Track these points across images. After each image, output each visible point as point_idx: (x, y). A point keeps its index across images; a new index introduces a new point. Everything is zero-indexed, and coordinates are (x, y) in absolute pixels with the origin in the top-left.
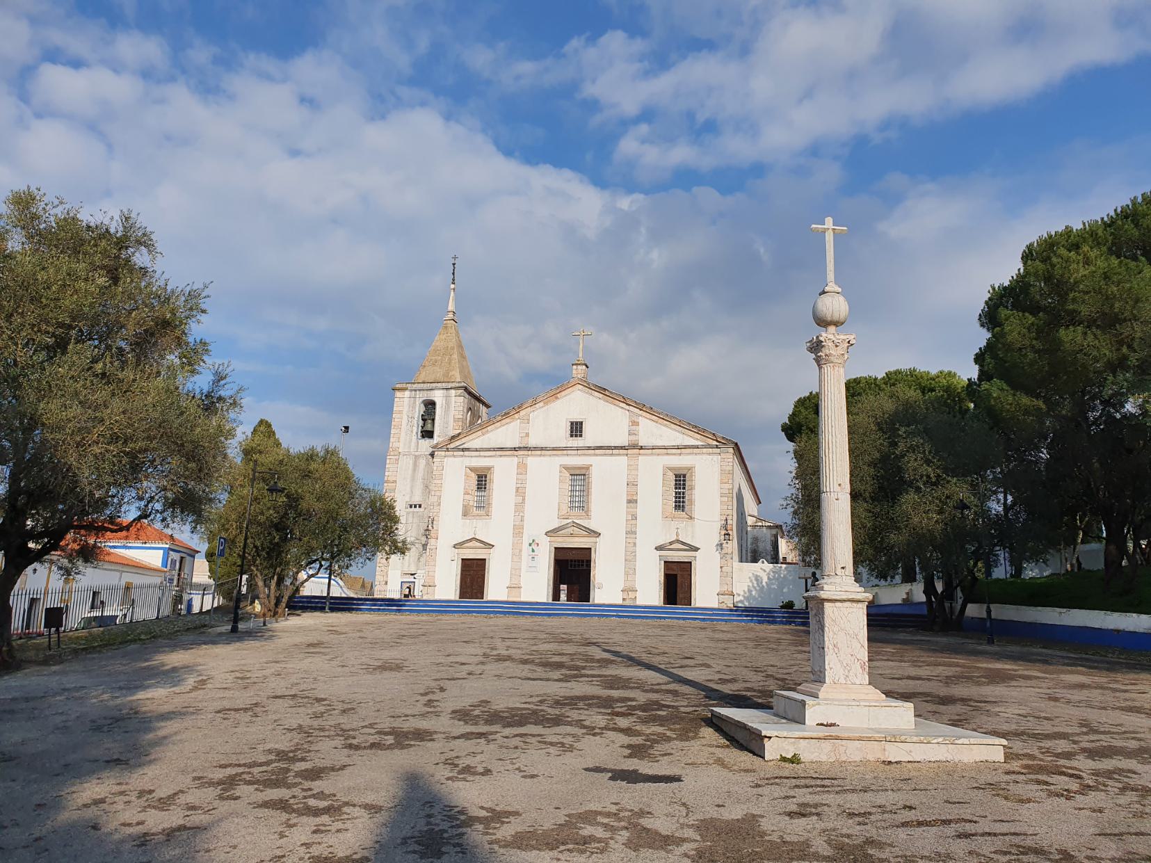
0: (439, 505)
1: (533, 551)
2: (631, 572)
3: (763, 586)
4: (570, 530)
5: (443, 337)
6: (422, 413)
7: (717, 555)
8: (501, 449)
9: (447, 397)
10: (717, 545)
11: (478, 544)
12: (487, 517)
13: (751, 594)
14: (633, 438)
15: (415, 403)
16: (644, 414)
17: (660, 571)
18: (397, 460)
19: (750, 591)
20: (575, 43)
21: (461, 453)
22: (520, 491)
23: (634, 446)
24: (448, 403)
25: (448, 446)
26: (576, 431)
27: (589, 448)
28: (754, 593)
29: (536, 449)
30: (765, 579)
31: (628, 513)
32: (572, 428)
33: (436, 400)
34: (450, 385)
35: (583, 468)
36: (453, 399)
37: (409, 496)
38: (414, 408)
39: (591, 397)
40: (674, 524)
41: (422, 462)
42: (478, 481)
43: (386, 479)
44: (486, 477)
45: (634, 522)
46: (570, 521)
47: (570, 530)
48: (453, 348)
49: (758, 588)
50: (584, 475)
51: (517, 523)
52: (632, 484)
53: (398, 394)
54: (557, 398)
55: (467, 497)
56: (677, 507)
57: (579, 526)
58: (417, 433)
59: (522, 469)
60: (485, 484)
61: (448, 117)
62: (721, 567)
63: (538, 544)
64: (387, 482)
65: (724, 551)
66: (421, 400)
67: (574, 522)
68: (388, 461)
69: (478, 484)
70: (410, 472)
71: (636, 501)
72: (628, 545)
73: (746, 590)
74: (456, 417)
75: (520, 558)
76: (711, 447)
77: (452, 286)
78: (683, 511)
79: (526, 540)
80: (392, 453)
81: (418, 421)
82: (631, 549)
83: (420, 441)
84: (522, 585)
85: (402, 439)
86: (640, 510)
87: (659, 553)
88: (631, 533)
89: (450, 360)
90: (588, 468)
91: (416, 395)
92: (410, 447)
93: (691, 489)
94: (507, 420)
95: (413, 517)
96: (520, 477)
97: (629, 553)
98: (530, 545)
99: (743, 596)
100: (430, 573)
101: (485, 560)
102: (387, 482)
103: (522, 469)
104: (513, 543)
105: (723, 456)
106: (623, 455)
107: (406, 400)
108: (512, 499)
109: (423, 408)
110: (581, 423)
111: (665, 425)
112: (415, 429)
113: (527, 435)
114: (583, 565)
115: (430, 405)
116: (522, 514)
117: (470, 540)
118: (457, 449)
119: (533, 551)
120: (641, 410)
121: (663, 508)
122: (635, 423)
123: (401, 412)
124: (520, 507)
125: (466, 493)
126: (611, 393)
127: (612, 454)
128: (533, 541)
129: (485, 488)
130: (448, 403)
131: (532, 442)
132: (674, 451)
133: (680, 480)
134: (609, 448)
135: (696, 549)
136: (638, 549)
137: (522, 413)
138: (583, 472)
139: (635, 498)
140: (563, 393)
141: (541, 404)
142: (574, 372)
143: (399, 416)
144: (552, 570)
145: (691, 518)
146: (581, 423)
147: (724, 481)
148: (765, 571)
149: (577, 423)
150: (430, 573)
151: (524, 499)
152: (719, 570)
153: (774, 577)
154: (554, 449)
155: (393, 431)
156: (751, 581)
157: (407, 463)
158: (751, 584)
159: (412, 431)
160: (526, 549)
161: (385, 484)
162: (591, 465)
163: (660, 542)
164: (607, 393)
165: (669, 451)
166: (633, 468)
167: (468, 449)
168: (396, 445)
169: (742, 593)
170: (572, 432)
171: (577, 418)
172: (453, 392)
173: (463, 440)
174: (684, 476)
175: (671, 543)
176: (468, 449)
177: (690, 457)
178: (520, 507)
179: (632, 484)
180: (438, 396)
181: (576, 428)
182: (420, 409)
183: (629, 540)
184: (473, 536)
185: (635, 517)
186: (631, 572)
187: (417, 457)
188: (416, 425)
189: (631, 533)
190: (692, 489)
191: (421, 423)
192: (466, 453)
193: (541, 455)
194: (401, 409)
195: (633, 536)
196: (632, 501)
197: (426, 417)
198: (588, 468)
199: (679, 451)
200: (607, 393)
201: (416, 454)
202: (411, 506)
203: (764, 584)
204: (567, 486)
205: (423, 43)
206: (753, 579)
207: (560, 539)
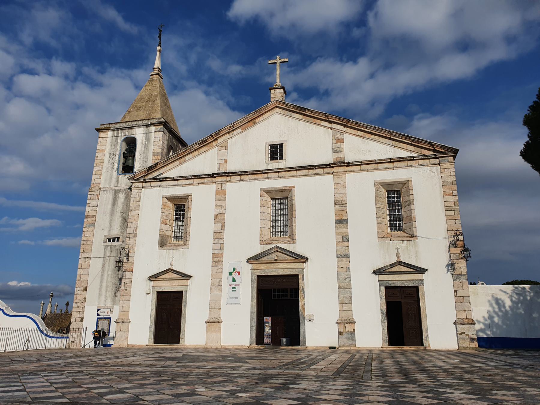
0: (135, 236)
1: (234, 280)
2: (346, 300)
3: (506, 311)
4: (274, 256)
5: (148, 88)
6: (124, 150)
7: (449, 277)
8: (199, 177)
9: (148, 133)
10: (448, 265)
11: (175, 276)
12: (184, 247)
13: (493, 322)
14: (338, 155)
15: (116, 141)
16: (349, 130)
17: (381, 298)
18: (98, 195)
19: (491, 317)
20: (260, 59)
21: (159, 183)
22: (219, 218)
23: (340, 163)
24: (148, 139)
25: (146, 178)
26: (276, 155)
27: (291, 169)
28: (496, 319)
29: (235, 174)
30: (508, 303)
31: (337, 235)
32: (271, 151)
33: (137, 136)
34: (149, 122)
35: (285, 190)
36: (153, 135)
37: (108, 229)
38: (116, 145)
39: (290, 119)
40: (394, 244)
41: (122, 197)
42: (176, 211)
43: (86, 214)
44: (184, 207)
45: (345, 244)
46: (274, 245)
47: (274, 256)
48: (156, 96)
49: (500, 314)
50: (286, 198)
51: (216, 252)
52: (340, 203)
53: (102, 134)
54: (255, 123)
55: (165, 227)
56: (393, 227)
57: (284, 251)
58: (118, 169)
59: (221, 194)
60: (184, 214)
61: (207, 93)
62: (455, 291)
63: (239, 273)
64: (88, 217)
65: (456, 272)
66: (123, 138)
67: (278, 247)
68: (89, 197)
69: (176, 215)
70: (110, 206)
71: (346, 221)
72: (341, 270)
73: (486, 315)
74: (156, 151)
75: (220, 290)
76: (428, 158)
77: (158, 48)
78: (400, 230)
79: (226, 269)
80: (93, 189)
81: (119, 157)
82: (344, 274)
83: (120, 177)
84: (222, 319)
85: (103, 176)
86: (352, 231)
87: (377, 278)
88: (343, 256)
89: (153, 106)
90: (289, 190)
91: (118, 134)
92: (110, 182)
93: (410, 204)
94: (205, 148)
95: (111, 251)
96: (219, 203)
97: (343, 279)
98: (231, 274)
99: (484, 324)
100: (125, 309)
101: (182, 292)
102: (88, 217)
103: (221, 194)
104: (212, 272)
105: (443, 166)
106: (328, 173)
107: (109, 140)
108: (211, 226)
109: (125, 147)
110: (281, 145)
111: (374, 140)
112: (116, 166)
113: (226, 161)
114: (286, 295)
115: (131, 143)
116: (221, 241)
117: (166, 272)
118: (155, 179)
119: (234, 280)
120: (345, 126)
121: (378, 227)
122: (339, 141)
123: (103, 151)
124: (219, 235)
125: (163, 223)
126: (311, 111)
127: (315, 175)
128: (234, 269)
129: (183, 218)
130: (148, 139)
131: (231, 168)
132: (386, 165)
133: (394, 197)
134: (312, 167)
135: (423, 271)
136: (352, 274)
137: (220, 140)
138: (284, 195)
139: (344, 218)
140: (261, 118)
141: (239, 130)
142: (272, 96)
143: (101, 154)
144: (255, 301)
145: (412, 236)
146: (281, 145)
147: (447, 193)
148: (505, 292)
149: (276, 145)
150: (125, 309)
151: (223, 226)
152: (453, 294)
153: (519, 299)
154: (254, 173)
155: (95, 169)
156: (491, 305)
157: (106, 198)
158: (490, 309)
159: (113, 168)
160: (226, 279)
161: (86, 220)
162: (294, 187)
163: (380, 265)
164: (308, 113)
165: (380, 166)
166: (339, 186)
167: (165, 179)
168: (97, 181)
169: (482, 320)
170: (271, 155)
171: (276, 140)
172: (153, 128)
173: (161, 171)
174: (398, 192)
175: (392, 266)
176: (165, 179)
177: (405, 170)
178: (219, 235)
179: (340, 203)
180: (139, 133)
181: (276, 151)
182: (121, 147)
183: (341, 265)
184: (170, 267)
185: (345, 239)
186: (346, 300)
187: (116, 192)
188: (117, 161)
189: (343, 256)
190: (410, 204)
191: (122, 160)
192: (164, 183)
193: (239, 181)
194: (104, 148)
195: (345, 259)
196: (341, 222)
197: (128, 155)
198: (289, 190)
199: (391, 165)
200: (308, 113)
201: (117, 188)
202: (109, 241)
203: (507, 308)
204: (268, 211)
205: (193, 58)
206: (493, 302)
207: (263, 266)
